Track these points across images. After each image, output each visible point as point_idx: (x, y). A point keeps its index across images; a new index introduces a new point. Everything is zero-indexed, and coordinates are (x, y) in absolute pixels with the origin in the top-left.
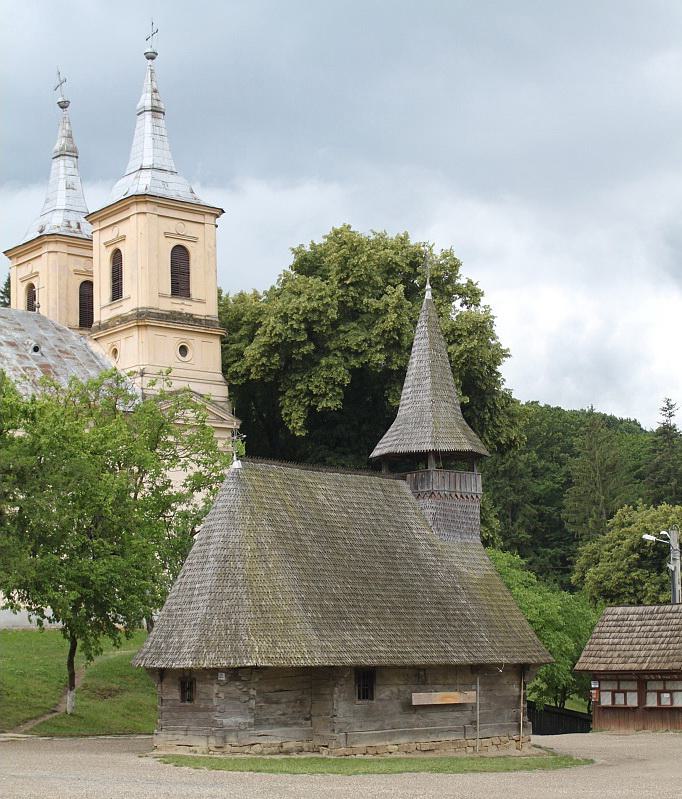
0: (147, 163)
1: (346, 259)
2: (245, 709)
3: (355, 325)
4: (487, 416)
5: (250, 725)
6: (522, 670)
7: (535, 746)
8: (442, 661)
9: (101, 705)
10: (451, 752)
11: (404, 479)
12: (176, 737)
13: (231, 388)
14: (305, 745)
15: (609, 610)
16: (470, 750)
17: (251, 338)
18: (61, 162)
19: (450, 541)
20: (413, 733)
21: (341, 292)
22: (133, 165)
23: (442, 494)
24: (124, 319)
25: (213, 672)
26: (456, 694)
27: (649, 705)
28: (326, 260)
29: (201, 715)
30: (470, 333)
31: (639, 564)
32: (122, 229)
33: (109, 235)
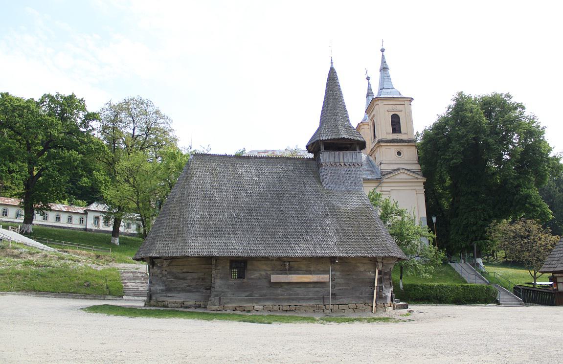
2: (160, 282)
5: (162, 291)
20: (278, 299)
23: (328, 164)
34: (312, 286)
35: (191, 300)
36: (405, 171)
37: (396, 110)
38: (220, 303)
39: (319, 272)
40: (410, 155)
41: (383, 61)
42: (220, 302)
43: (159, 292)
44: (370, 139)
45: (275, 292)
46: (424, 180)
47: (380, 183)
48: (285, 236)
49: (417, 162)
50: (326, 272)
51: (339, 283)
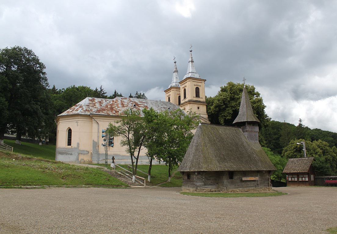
0: (191, 71)
1: (231, 88)
3: (233, 101)
4: (262, 120)
5: (203, 185)
6: (269, 172)
7: (273, 190)
8: (249, 170)
9: (177, 180)
10: (252, 192)
11: (240, 128)
12: (187, 188)
13: (208, 115)
14: (217, 190)
15: (290, 159)
16: (257, 191)
17: (212, 105)
18: (175, 73)
19: (250, 140)
21: (230, 95)
22: (188, 72)
24: (186, 102)
25: (194, 172)
26: (253, 178)
27: (300, 180)
28: (227, 89)
29: (192, 183)
30: (258, 102)
31: (296, 151)
32: (186, 84)
33: (183, 86)
37: (198, 85)
43: (201, 185)
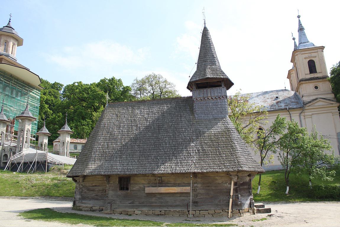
34: (178, 195)
35: (97, 206)
36: (322, 100)
38: (111, 209)
39: (184, 185)
40: (326, 87)
41: (300, 24)
42: (111, 207)
44: (296, 80)
45: (151, 200)
46: (338, 104)
47: (303, 110)
48: (156, 157)
49: (331, 92)
50: (188, 185)
51: (200, 193)
